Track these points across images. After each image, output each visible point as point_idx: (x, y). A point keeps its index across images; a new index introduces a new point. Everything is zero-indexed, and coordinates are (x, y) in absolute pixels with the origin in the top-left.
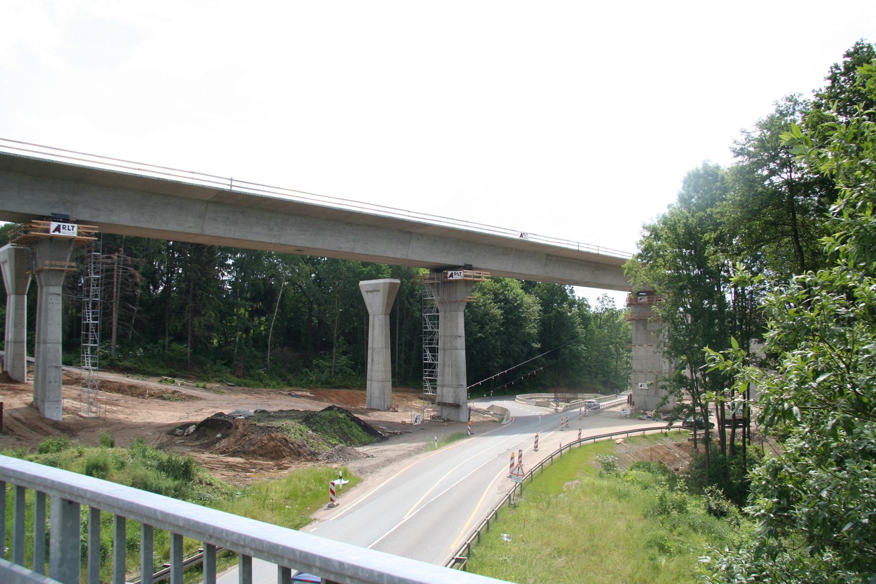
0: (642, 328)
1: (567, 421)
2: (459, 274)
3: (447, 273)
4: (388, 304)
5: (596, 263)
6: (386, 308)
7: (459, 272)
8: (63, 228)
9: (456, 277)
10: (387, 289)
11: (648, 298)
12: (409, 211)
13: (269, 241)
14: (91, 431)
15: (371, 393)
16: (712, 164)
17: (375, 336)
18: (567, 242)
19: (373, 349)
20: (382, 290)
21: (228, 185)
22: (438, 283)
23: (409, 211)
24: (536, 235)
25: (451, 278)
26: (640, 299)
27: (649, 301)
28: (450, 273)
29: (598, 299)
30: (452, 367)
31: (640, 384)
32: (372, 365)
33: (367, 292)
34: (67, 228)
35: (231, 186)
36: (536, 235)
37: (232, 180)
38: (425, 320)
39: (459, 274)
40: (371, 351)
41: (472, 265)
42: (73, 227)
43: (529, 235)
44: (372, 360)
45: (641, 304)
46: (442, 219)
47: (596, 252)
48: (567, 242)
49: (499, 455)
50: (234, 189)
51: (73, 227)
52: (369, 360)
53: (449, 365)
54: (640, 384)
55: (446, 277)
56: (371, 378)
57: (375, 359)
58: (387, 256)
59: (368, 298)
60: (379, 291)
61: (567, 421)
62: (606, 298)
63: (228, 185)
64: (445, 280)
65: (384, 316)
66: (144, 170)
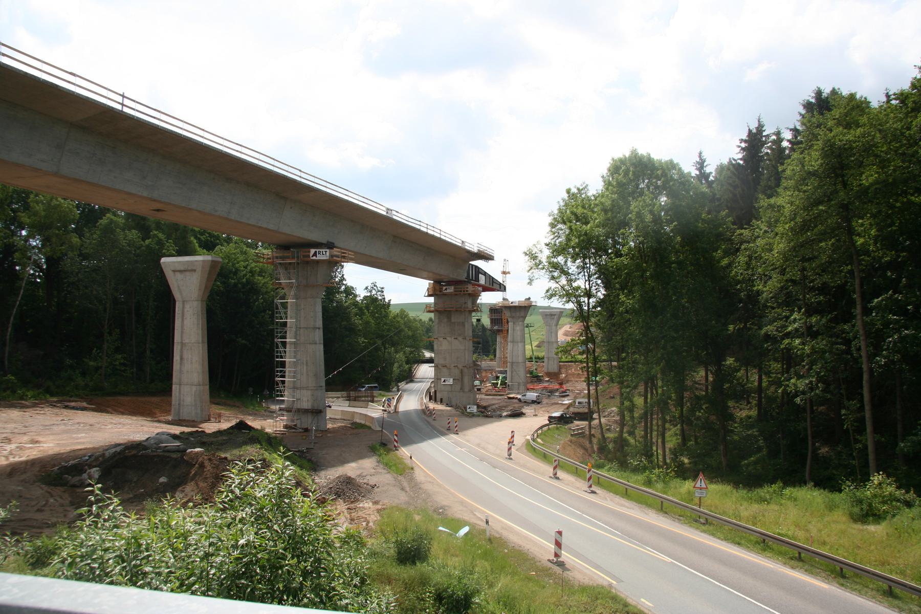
0: (445, 320)
1: (449, 423)
2: (324, 253)
3: (309, 252)
4: (206, 287)
6: (204, 293)
7: (324, 250)
10: (208, 269)
11: (455, 288)
12: (300, 171)
13: (140, 194)
14: (646, 514)
15: (180, 400)
16: (642, 151)
17: (185, 328)
18: (419, 223)
19: (182, 344)
20: (199, 269)
21: (119, 103)
22: (298, 263)
23: (300, 171)
24: (398, 212)
25: (314, 258)
26: (446, 289)
27: (455, 291)
28: (312, 251)
29: (367, 288)
30: (307, 365)
32: (181, 364)
33: (174, 271)
35: (123, 105)
36: (398, 212)
37: (123, 96)
38: (277, 308)
39: (324, 253)
40: (179, 347)
41: (334, 244)
42: (326, 252)
43: (394, 213)
44: (182, 359)
45: (445, 295)
47: (438, 235)
48: (419, 223)
49: (495, 467)
50: (126, 110)
51: (326, 252)
52: (176, 357)
53: (303, 363)
55: (309, 256)
56: (180, 380)
57: (185, 356)
58: (260, 225)
59: (175, 282)
60: (195, 271)
61: (449, 423)
62: (375, 288)
63: (119, 103)
64: (306, 259)
65: (200, 302)
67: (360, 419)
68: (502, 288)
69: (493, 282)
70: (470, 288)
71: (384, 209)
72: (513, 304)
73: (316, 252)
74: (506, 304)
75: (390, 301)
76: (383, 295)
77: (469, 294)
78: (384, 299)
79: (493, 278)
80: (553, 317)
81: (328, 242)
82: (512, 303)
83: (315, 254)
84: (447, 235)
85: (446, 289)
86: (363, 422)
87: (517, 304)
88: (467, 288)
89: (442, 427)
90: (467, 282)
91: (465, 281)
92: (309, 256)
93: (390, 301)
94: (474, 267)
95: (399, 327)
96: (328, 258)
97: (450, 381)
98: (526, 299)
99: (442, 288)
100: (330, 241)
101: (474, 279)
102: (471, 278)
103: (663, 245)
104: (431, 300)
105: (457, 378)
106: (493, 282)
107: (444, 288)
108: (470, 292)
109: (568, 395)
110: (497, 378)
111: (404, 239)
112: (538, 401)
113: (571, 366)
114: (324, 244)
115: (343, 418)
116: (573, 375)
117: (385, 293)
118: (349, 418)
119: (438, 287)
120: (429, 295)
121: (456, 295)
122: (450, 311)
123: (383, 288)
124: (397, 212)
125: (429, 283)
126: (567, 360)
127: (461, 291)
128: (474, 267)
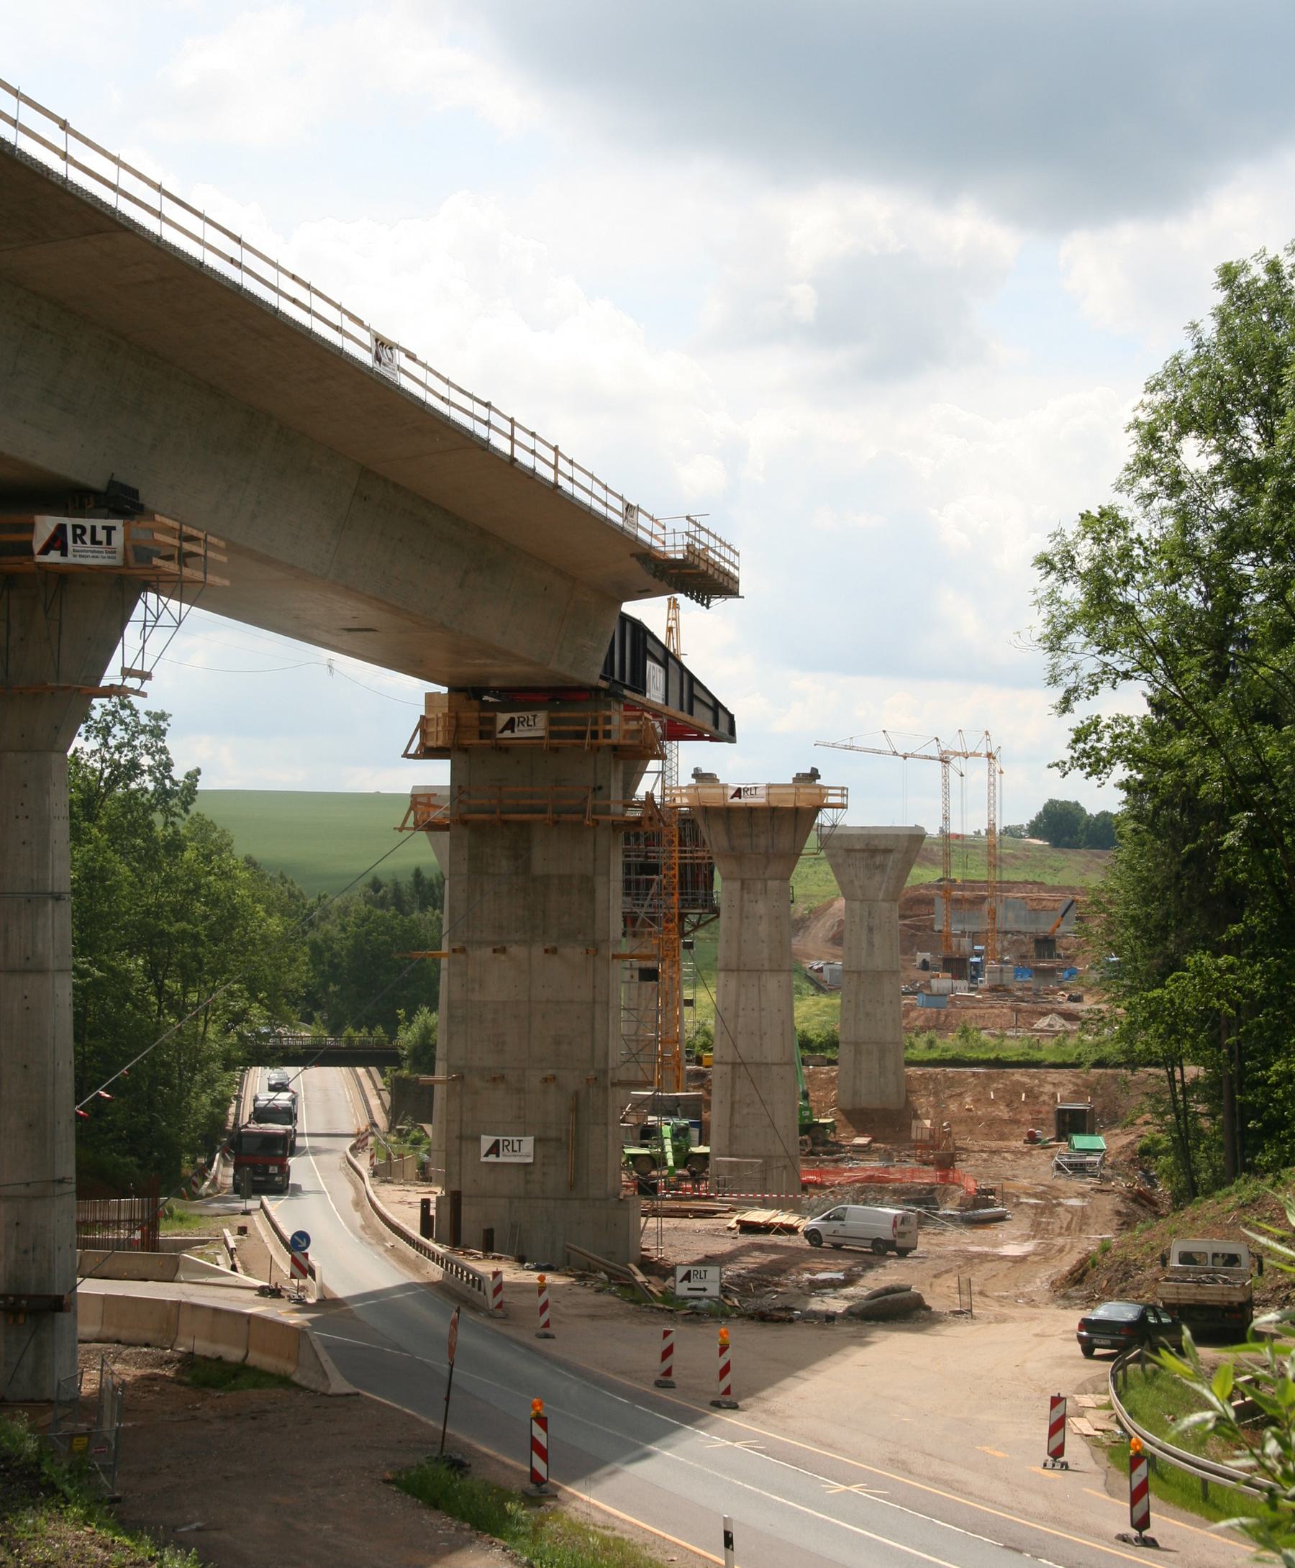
2: (101, 535)
3: (30, 528)
5: (446, 510)
7: (99, 523)
8: (75, 536)
9: (80, 555)
11: (552, 722)
12: (64, 125)
23: (64, 125)
25: (54, 557)
26: (510, 725)
27: (553, 735)
28: (46, 525)
31: (487, 1142)
34: (87, 538)
39: (101, 535)
41: (135, 493)
42: (109, 530)
45: (503, 749)
46: (171, 210)
51: (109, 530)
54: (487, 1142)
55: (27, 549)
62: (125, 713)
66: (453, 405)
67: (213, 1339)
68: (723, 728)
69: (692, 697)
70: (618, 724)
71: (367, 339)
72: (745, 800)
73: (61, 528)
74: (710, 796)
75: (194, 776)
76: (163, 751)
77: (615, 748)
78: (168, 765)
79: (693, 679)
80: (878, 859)
81: (112, 484)
82: (738, 793)
83: (57, 541)
84: (579, 476)
85: (510, 725)
86: (233, 1354)
87: (759, 800)
88: (608, 720)
89: (622, 1373)
90: (608, 693)
91: (597, 689)
92: (29, 545)
93: (194, 776)
94: (628, 626)
95: (231, 893)
96: (118, 561)
97: (524, 1150)
98: (800, 778)
99: (492, 721)
100: (122, 478)
101: (627, 682)
102: (617, 677)
103: (1086, 551)
104: (438, 773)
105: (553, 1133)
106: (692, 697)
107: (503, 718)
108: (616, 739)
109: (1001, 1218)
110: (648, 1134)
111: (396, 486)
112: (900, 1243)
113: (962, 1082)
114: (95, 493)
115: (111, 1332)
116: (970, 1120)
117: (169, 742)
118: (149, 1336)
119: (471, 715)
120: (428, 752)
121: (556, 750)
122: (524, 825)
123: (162, 716)
124: (411, 357)
125: (430, 697)
126: (934, 1055)
127: (581, 735)
128: (628, 626)
